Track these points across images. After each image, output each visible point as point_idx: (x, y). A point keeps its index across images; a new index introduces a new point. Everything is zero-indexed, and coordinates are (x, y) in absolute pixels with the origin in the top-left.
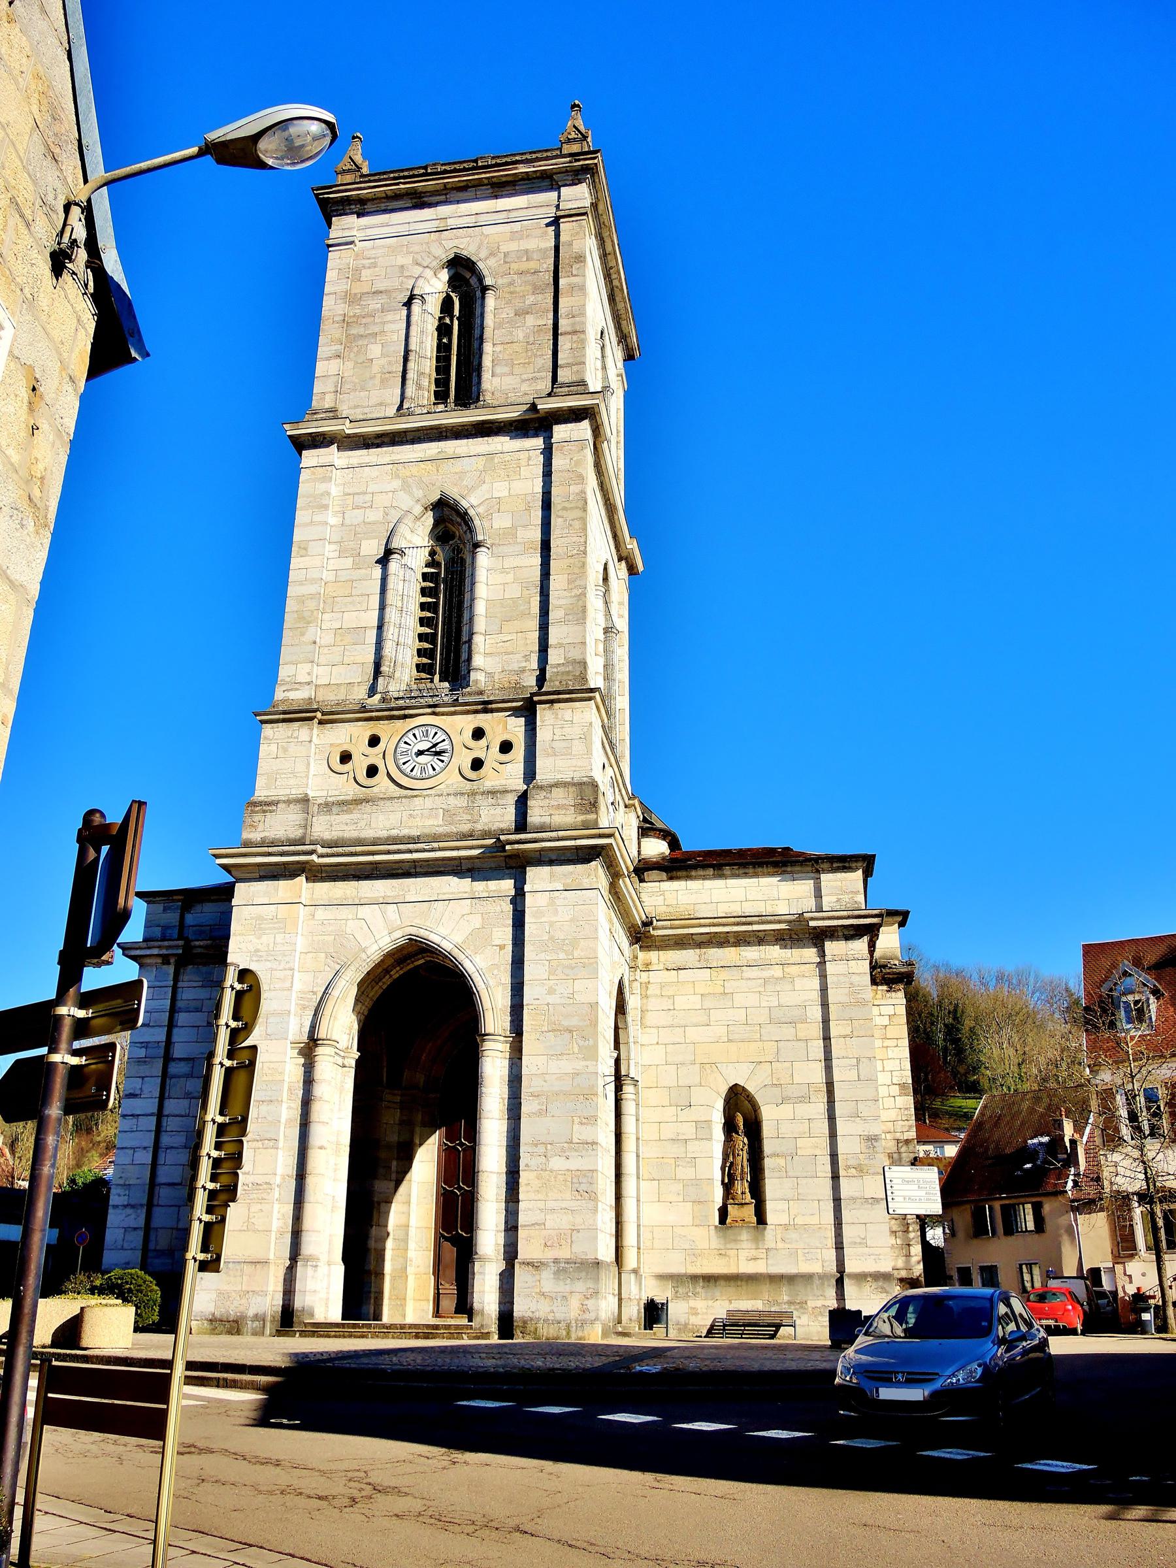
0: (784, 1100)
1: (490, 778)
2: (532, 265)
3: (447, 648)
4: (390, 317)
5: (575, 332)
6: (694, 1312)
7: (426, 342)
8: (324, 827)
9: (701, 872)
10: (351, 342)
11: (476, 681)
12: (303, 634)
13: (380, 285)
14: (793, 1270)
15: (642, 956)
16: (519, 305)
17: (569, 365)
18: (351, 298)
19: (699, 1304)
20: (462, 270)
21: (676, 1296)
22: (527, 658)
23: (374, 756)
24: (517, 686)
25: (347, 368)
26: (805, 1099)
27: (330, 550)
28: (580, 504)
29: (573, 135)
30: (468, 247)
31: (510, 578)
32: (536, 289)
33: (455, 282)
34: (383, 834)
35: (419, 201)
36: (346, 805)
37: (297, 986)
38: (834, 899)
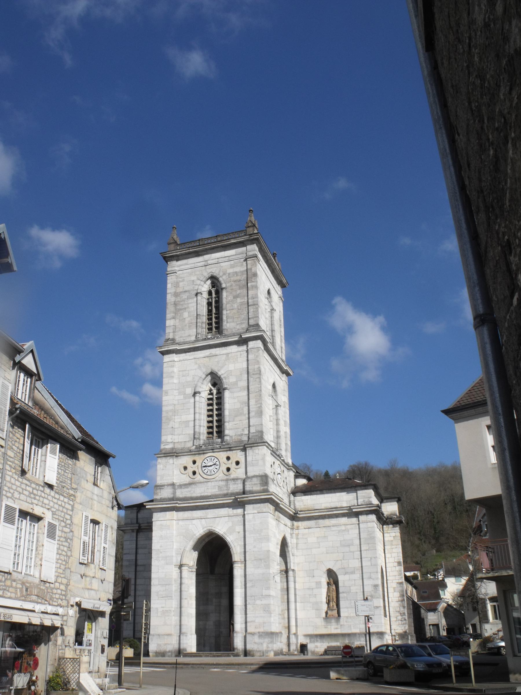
0: (346, 573)
1: (233, 474)
2: (238, 278)
3: (217, 426)
4: (190, 301)
5: (254, 305)
6: (317, 647)
7: (204, 310)
8: (180, 493)
9: (315, 492)
10: (177, 311)
11: (227, 440)
12: (168, 425)
13: (186, 289)
14: (350, 632)
15: (295, 523)
16: (234, 293)
17: (253, 318)
18: (176, 295)
19: (318, 644)
20: (214, 281)
21: (310, 642)
22: (243, 430)
23: (194, 468)
24: (241, 441)
25: (177, 322)
26: (353, 573)
27: (176, 392)
28: (258, 372)
29: (250, 224)
30: (215, 271)
31: (236, 400)
32: (240, 288)
33: (213, 285)
34: (199, 495)
35: (197, 254)
36: (186, 485)
37: (175, 547)
38: (362, 500)
